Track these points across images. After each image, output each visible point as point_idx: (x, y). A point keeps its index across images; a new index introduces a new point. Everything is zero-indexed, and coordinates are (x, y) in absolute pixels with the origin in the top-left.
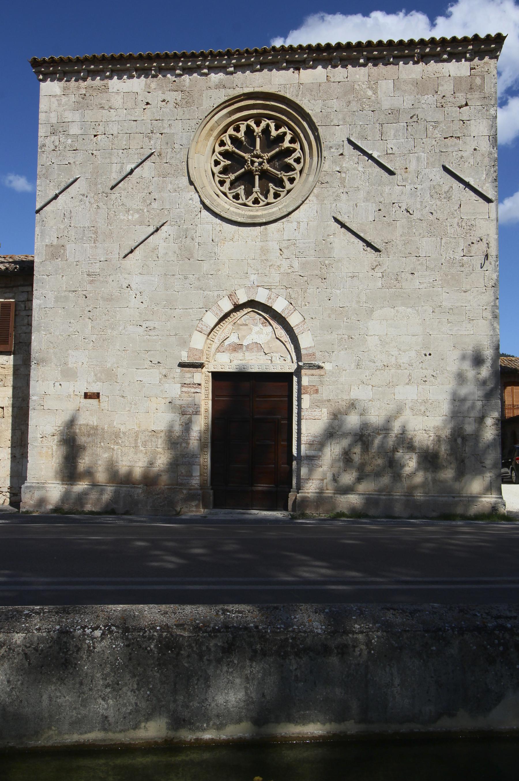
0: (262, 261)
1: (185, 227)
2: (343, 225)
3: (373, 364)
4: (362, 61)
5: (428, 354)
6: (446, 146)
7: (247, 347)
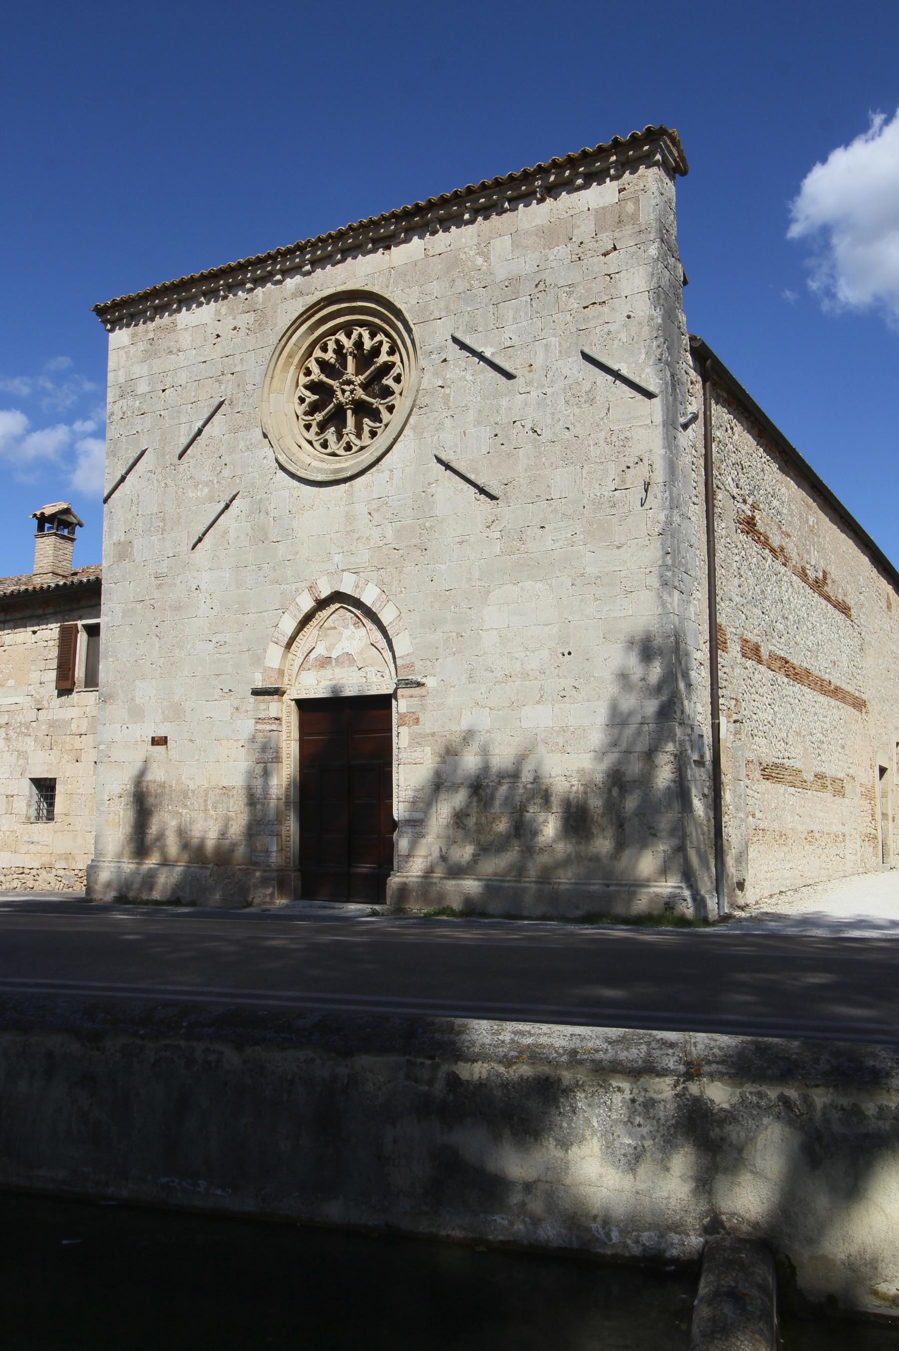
0: (348, 532)
1: (258, 497)
2: (448, 467)
3: (491, 674)
4: (467, 216)
5: (566, 654)
6: (586, 320)
7: (337, 659)
